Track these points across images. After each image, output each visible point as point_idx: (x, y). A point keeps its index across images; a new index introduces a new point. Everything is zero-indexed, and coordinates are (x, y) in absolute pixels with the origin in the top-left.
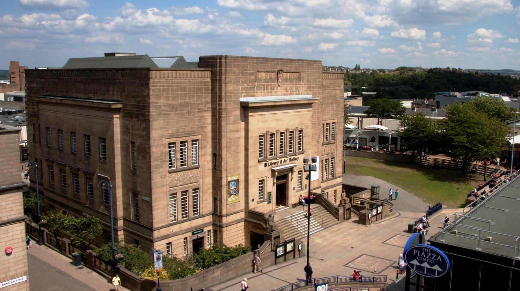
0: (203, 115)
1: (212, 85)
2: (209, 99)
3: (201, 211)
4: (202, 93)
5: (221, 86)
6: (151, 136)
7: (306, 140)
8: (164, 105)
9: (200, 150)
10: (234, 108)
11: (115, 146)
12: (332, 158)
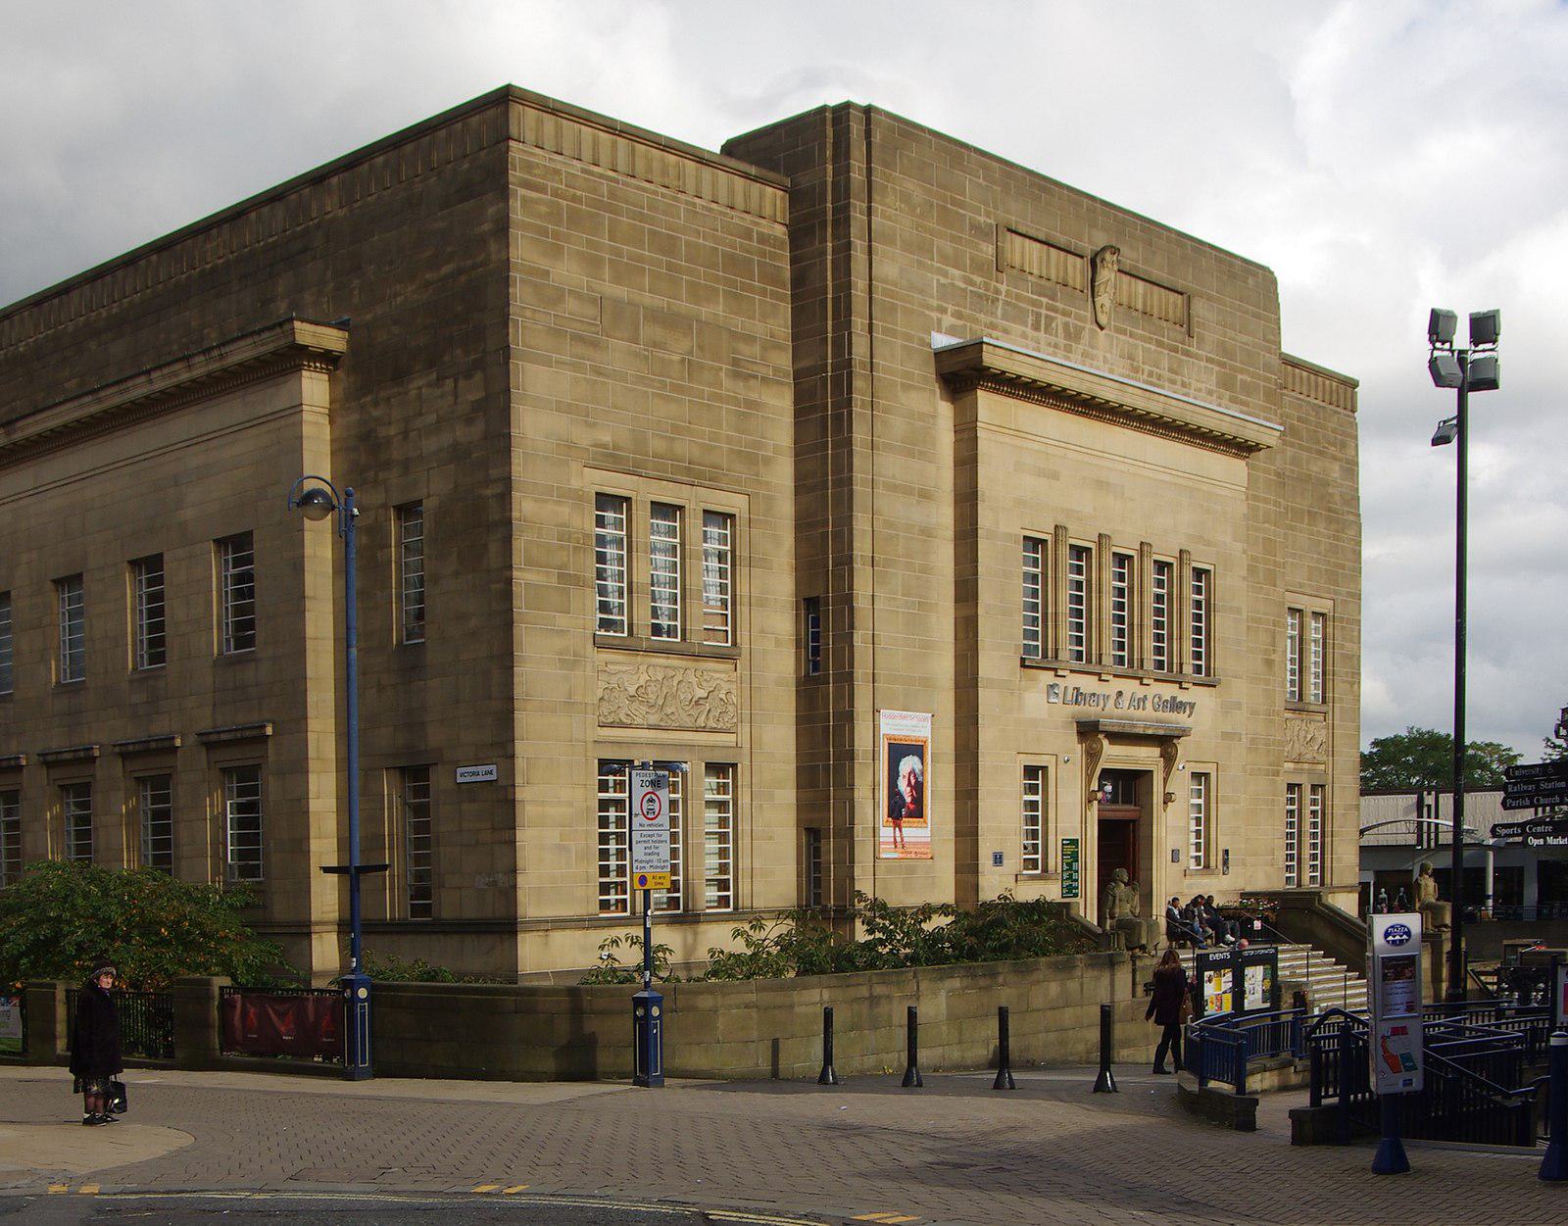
0: (754, 396)
1: (793, 261)
2: (780, 323)
3: (744, 887)
4: (751, 289)
5: (844, 250)
6: (514, 432)
7: (1223, 625)
8: (579, 296)
9: (743, 571)
10: (906, 375)
11: (308, 551)
12: (1314, 788)
